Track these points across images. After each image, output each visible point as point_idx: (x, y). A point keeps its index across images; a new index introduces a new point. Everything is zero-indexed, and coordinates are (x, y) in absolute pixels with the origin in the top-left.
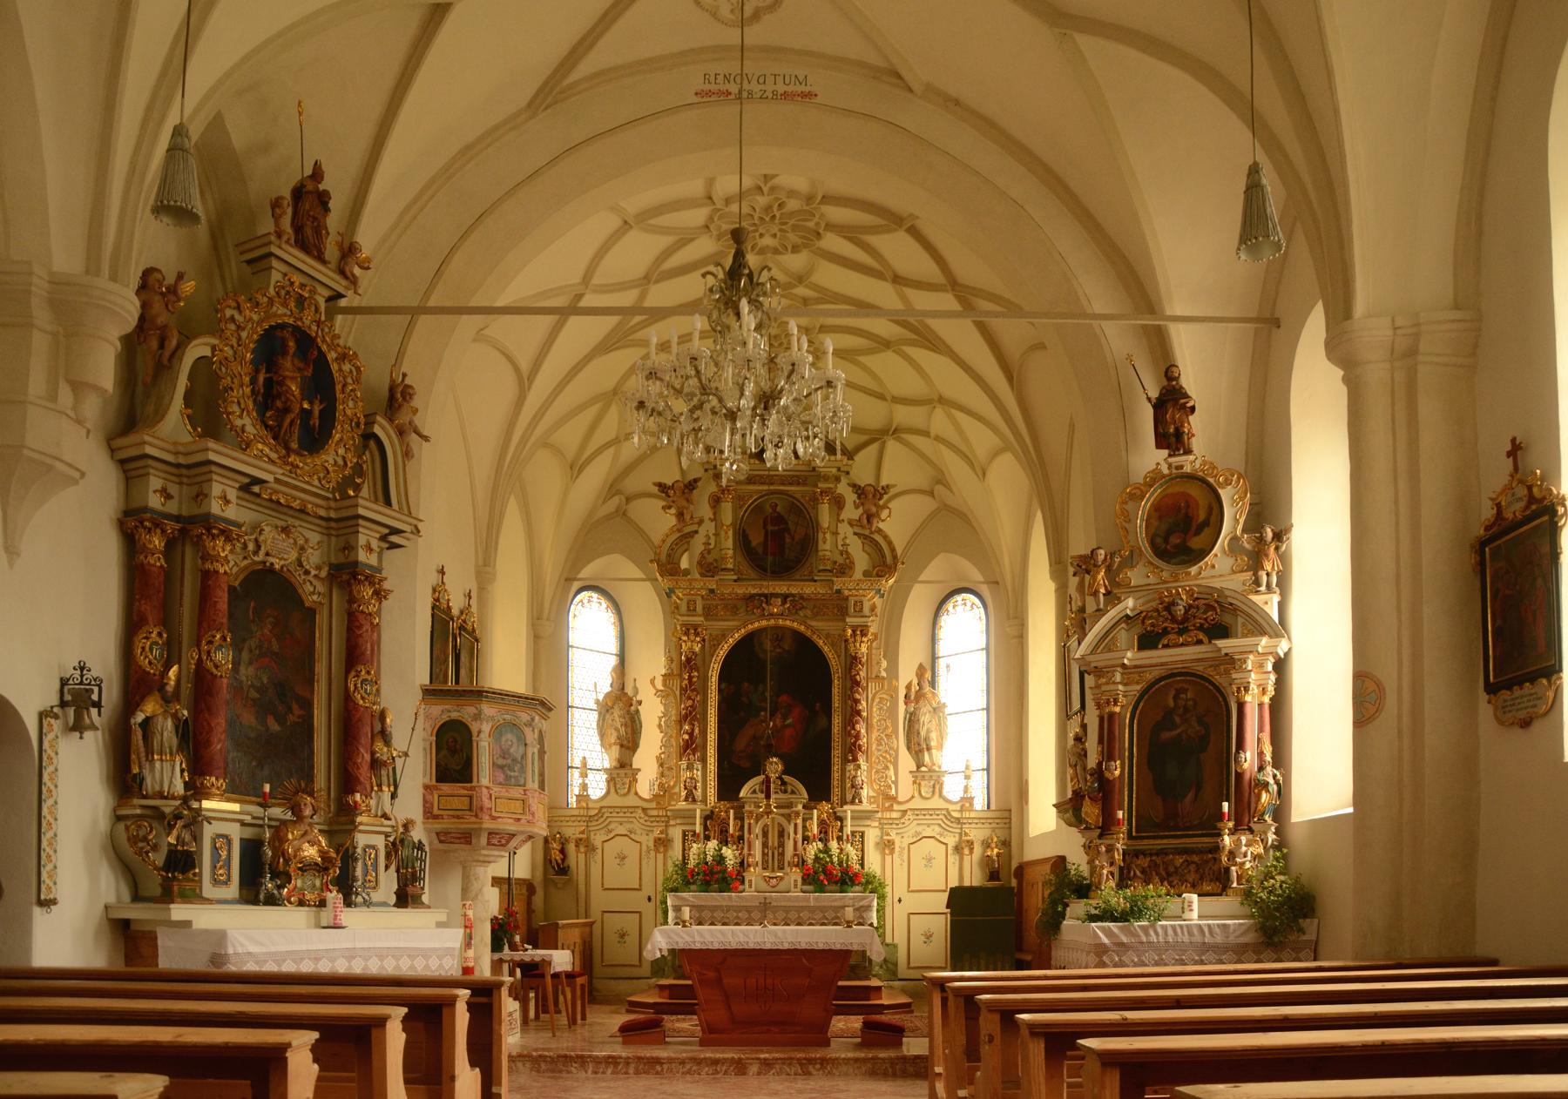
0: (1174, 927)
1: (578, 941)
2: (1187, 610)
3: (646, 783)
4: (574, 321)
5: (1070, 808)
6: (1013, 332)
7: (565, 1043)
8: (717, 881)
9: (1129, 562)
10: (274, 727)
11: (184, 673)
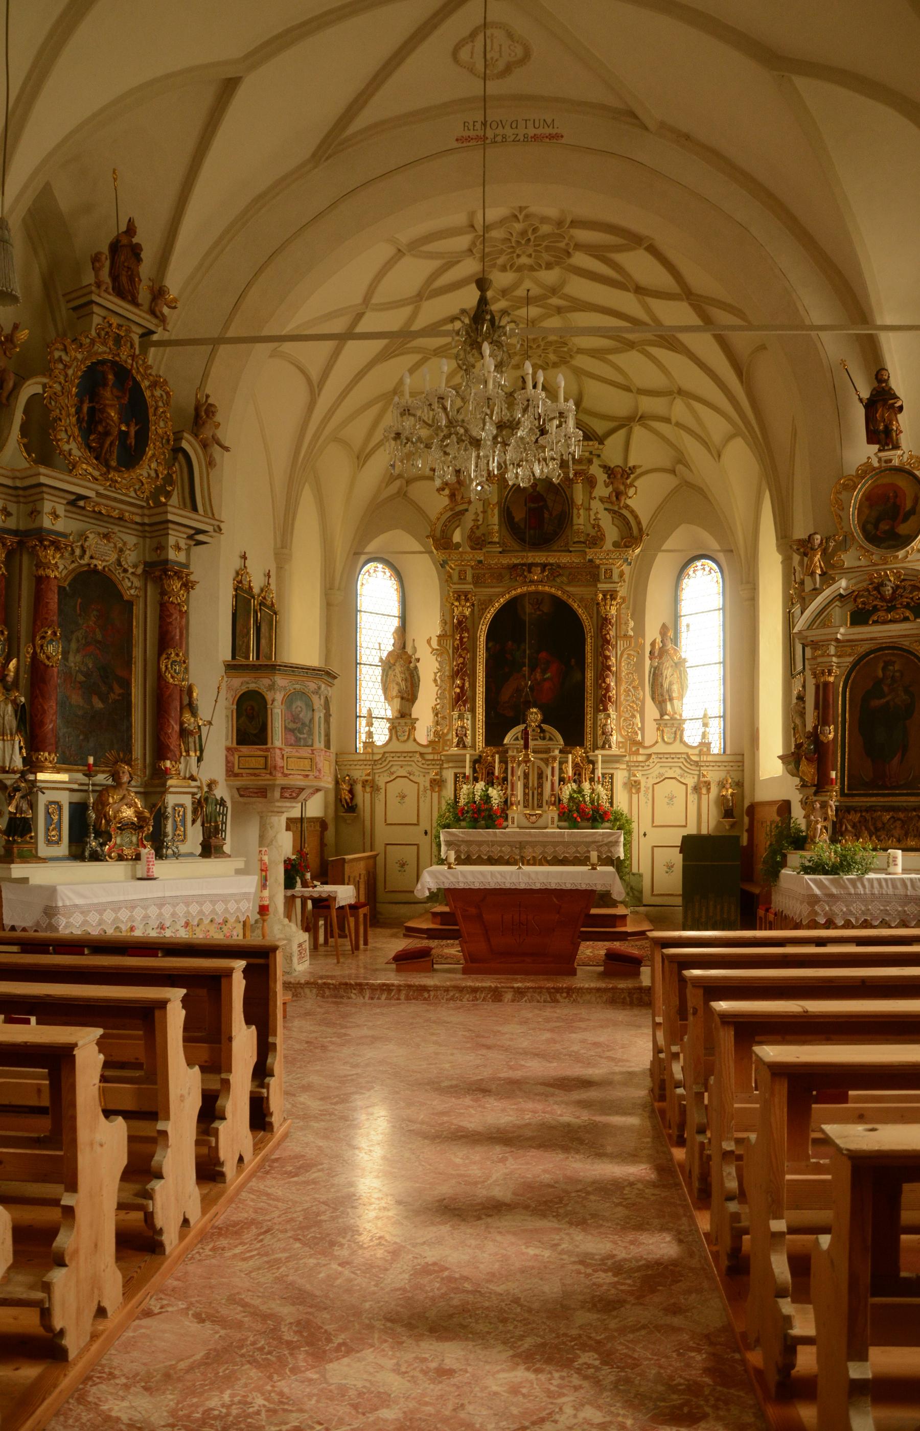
0: (879, 880)
1: (363, 872)
2: (895, 590)
3: (423, 733)
4: (351, 345)
5: (793, 759)
6: (742, 341)
7: (348, 970)
8: (484, 818)
9: (843, 546)
10: (99, 705)
11: (22, 664)
